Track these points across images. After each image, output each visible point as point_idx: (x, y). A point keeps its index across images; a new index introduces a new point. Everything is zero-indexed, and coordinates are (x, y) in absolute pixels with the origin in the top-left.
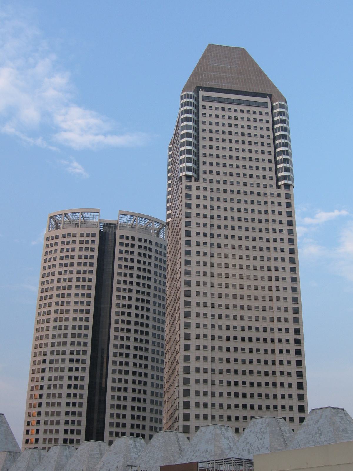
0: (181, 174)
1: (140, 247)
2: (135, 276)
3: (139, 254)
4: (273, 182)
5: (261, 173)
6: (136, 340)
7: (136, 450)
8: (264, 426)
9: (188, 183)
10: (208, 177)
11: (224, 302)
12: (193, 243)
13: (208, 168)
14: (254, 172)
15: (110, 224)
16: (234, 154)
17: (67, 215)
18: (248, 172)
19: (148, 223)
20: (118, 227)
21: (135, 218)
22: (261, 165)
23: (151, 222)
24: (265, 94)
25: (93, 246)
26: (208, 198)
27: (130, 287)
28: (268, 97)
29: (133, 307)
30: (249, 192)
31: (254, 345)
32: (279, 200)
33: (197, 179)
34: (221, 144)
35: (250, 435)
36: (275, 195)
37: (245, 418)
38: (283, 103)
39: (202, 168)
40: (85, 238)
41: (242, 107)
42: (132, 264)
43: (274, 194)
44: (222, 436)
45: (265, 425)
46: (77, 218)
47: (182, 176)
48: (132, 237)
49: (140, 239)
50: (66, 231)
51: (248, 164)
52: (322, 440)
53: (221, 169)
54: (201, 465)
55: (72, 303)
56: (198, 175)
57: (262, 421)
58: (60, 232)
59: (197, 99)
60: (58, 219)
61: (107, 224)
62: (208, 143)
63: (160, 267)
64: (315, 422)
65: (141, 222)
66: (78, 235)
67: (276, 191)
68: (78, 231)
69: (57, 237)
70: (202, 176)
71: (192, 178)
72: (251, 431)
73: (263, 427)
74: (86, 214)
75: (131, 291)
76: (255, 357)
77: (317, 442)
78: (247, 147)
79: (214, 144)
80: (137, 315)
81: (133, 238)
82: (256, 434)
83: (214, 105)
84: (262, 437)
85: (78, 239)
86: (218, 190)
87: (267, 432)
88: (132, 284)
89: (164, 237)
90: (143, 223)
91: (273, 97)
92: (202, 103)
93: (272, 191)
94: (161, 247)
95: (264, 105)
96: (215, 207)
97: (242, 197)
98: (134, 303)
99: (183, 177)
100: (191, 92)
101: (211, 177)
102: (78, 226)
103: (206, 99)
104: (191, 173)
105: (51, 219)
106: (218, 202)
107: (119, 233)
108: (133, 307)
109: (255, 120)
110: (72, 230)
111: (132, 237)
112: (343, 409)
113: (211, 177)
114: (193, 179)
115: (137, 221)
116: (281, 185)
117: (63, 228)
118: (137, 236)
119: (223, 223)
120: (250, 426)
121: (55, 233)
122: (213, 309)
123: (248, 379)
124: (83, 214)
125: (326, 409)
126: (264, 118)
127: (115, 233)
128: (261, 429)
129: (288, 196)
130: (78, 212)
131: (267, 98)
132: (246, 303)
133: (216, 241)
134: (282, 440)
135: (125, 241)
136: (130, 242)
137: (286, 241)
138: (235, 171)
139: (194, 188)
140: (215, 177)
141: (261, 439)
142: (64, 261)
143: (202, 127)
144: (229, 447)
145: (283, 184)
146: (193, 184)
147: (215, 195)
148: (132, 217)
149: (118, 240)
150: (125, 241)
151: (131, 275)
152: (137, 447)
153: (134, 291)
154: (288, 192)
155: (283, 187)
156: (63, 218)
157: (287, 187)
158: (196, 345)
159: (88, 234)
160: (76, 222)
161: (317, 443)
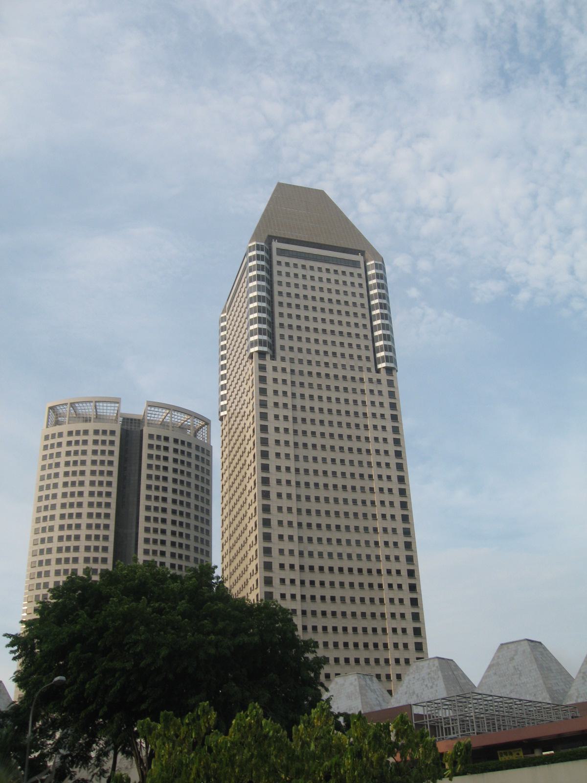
0: (252, 350)
1: (176, 451)
2: (170, 490)
3: (175, 461)
4: (371, 365)
5: (355, 352)
6: (175, 491)
8: (433, 669)
9: (262, 362)
10: (288, 355)
11: (314, 520)
12: (271, 442)
13: (287, 343)
14: (347, 351)
15: (132, 420)
16: (320, 326)
17: (73, 405)
20: (146, 424)
21: (168, 411)
22: (354, 341)
23: (189, 417)
24: (355, 250)
25: (112, 448)
26: (289, 382)
27: (163, 527)
29: (169, 511)
30: (340, 376)
31: (357, 579)
32: (380, 388)
33: (273, 357)
34: (302, 313)
35: (413, 683)
37: (407, 661)
38: (381, 263)
39: (279, 342)
40: (100, 438)
41: (327, 266)
42: (165, 474)
43: (373, 379)
44: (367, 688)
45: (435, 668)
46: (88, 410)
49: (176, 441)
50: (74, 427)
51: (338, 339)
52: (523, 681)
53: (305, 346)
54: (418, 710)
55: (84, 527)
56: (274, 351)
57: (429, 664)
58: (64, 428)
59: (269, 252)
60: (61, 410)
61: (128, 419)
62: (286, 311)
63: (203, 478)
64: (508, 660)
66: (91, 432)
67: (375, 376)
68: (91, 426)
69: (60, 435)
70: (279, 353)
72: (414, 678)
73: (431, 671)
74: (101, 404)
75: (164, 510)
76: (358, 594)
77: (517, 685)
78: (336, 318)
79: (294, 312)
80: (174, 522)
81: (166, 439)
82: (422, 681)
84: (433, 684)
85: (91, 438)
86: (301, 373)
87: (439, 677)
88: (167, 480)
90: (179, 418)
91: (366, 255)
92: (276, 258)
93: (370, 375)
95: (355, 264)
96: (298, 395)
97: (333, 383)
98: (169, 527)
99: (382, 369)
100: (263, 242)
101: (292, 355)
102: (90, 421)
103: (281, 252)
104: (265, 349)
105: (51, 410)
106: (302, 389)
107: (146, 431)
108: (169, 533)
109: (345, 283)
110: (82, 426)
112: (540, 643)
113: (292, 355)
114: (268, 357)
117: (69, 423)
118: (172, 436)
119: (309, 416)
120: (411, 671)
121: (57, 429)
122: (301, 530)
123: (350, 623)
124: (97, 404)
125: (522, 643)
126: (357, 281)
127: (142, 431)
128: (429, 674)
129: (391, 383)
130: (92, 402)
131: (358, 255)
133: (301, 440)
134: (458, 688)
135: (155, 442)
136: (163, 444)
137: (390, 441)
138: (322, 348)
139: (269, 368)
140: (296, 355)
141: (432, 687)
142: (71, 469)
143: (277, 289)
144: (378, 703)
146: (269, 363)
147: (298, 379)
148: (164, 411)
149: (146, 441)
151: (164, 500)
153: (169, 511)
154: (391, 378)
155: (383, 372)
156: (68, 409)
157: (389, 371)
159: (104, 432)
160: (85, 416)
161: (517, 687)
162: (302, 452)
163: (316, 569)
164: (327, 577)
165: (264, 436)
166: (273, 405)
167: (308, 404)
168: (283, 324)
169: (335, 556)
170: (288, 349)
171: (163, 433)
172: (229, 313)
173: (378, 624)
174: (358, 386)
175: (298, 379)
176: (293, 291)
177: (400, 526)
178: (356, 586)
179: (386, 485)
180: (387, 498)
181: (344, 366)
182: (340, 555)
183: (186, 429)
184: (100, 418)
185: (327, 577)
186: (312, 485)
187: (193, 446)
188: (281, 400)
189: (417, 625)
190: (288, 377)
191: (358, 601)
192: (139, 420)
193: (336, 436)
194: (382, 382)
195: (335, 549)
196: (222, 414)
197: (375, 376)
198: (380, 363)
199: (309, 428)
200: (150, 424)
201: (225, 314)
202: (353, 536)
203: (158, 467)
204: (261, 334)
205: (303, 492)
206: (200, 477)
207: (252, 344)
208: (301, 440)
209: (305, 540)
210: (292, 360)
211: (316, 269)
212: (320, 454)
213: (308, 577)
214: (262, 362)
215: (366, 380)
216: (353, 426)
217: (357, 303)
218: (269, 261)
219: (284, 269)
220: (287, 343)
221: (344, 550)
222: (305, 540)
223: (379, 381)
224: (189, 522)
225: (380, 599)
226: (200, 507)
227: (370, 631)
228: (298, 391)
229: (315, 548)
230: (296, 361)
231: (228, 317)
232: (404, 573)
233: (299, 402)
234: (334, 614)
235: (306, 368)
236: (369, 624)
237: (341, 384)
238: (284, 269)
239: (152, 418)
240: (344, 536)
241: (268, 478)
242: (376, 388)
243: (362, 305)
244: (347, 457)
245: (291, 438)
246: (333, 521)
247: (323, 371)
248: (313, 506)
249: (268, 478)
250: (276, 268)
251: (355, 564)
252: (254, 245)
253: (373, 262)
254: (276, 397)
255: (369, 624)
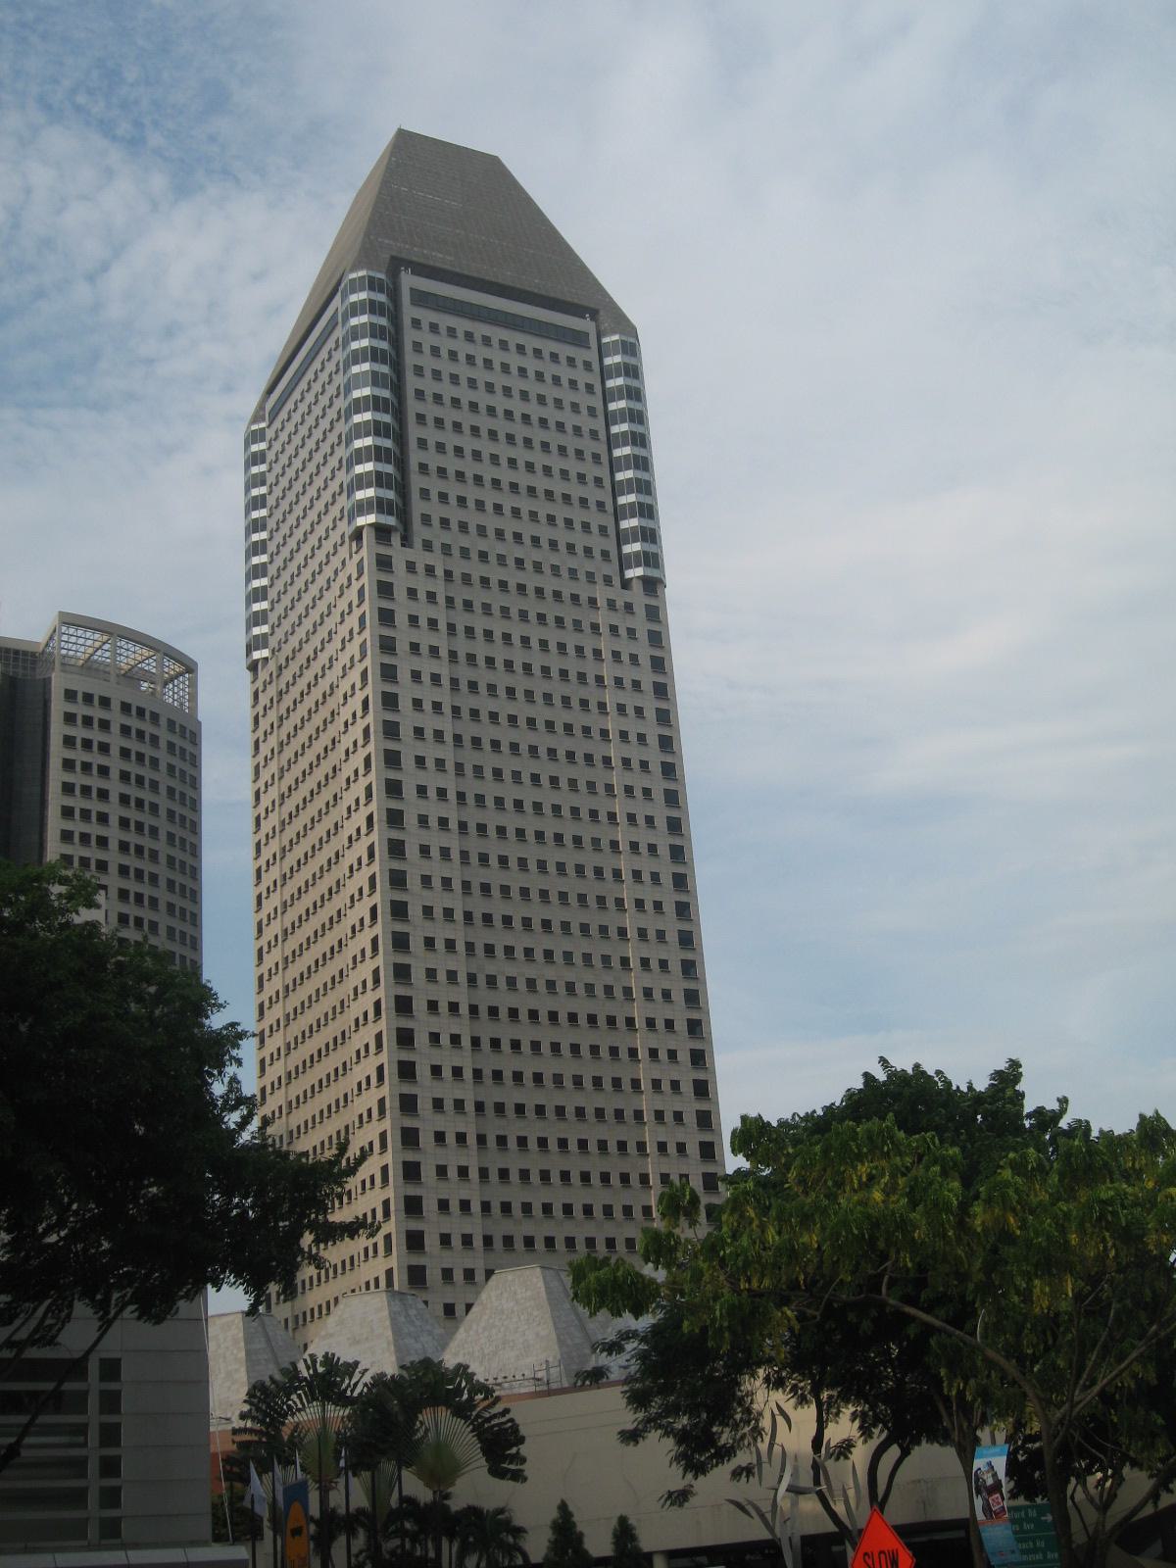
0: (361, 521)
4: (612, 569)
7: (412, 1329)
9: (383, 550)
10: (439, 537)
11: (498, 908)
15: (17, 652)
16: (506, 476)
18: (563, 537)
19: (97, 644)
28: (587, 315)
33: (406, 541)
36: (617, 607)
38: (632, 340)
39: (418, 507)
42: (103, 808)
47: (362, 527)
48: (101, 698)
49: (126, 708)
59: (394, 294)
63: (183, 795)
65: (73, 639)
67: (621, 597)
70: (420, 532)
71: (393, 534)
78: (538, 458)
81: (105, 702)
83: (446, 321)
89: (187, 697)
90: (130, 655)
92: (409, 311)
94: (183, 736)
95: (578, 339)
99: (634, 580)
100: (380, 272)
101: (446, 537)
103: (421, 299)
104: (391, 521)
107: (58, 683)
111: (101, 698)
113: (446, 537)
114: (396, 539)
115: (60, 637)
116: (632, 579)
123: (573, 1132)
131: (585, 318)
132: (556, 914)
133: (468, 730)
135: (80, 710)
136: (97, 713)
139: (399, 565)
145: (638, 577)
146: (399, 554)
149: (58, 707)
150: (80, 710)
151: (104, 748)
152: (413, 1322)
155: (637, 587)
158: (430, 1033)
162: (470, 758)
163: (503, 1013)
164: (526, 1033)
165: (390, 717)
166: (407, 648)
167: (481, 650)
168: (481, 477)
169: (541, 986)
170: (457, 529)
171: (98, 689)
172: (277, 424)
173: (628, 1133)
174: (587, 617)
175: (461, 594)
176: (448, 390)
177: (672, 926)
178: (545, 1048)
179: (644, 837)
180: (646, 865)
181: (555, 569)
182: (531, 984)
183: (139, 680)
184: (97, 670)
185: (526, 1033)
186: (492, 832)
187: (163, 721)
188: (426, 639)
189: (707, 1137)
190: (439, 587)
191: (607, 1084)
192: (33, 654)
193: (484, 716)
194: (636, 608)
195: (542, 972)
196: (256, 655)
197: (621, 597)
198: (630, 567)
199: (484, 704)
200: (66, 665)
201: (263, 425)
202: (579, 946)
203: (86, 767)
204: (382, 487)
205: (475, 845)
206: (177, 793)
207: (362, 508)
208: (468, 730)
209: (480, 950)
210: (446, 549)
211: (425, 326)
212: (508, 763)
213: (487, 1030)
214: (383, 550)
215: (601, 602)
216: (501, 692)
217: (497, 409)
218: (395, 318)
219: (428, 340)
220: (437, 511)
221: (560, 974)
222: (480, 950)
223: (629, 607)
224: (156, 895)
225: (633, 1080)
226: (177, 861)
227: (612, 1147)
228: (462, 620)
229: (501, 968)
230: (456, 552)
231: (270, 434)
232: (681, 1026)
233: (462, 646)
234: (520, 1109)
235: (477, 570)
236: (612, 1134)
237: (551, 610)
238: (428, 340)
239: (71, 653)
240: (559, 944)
241: (401, 812)
242: (623, 622)
243: (594, 434)
244: (565, 772)
245: (446, 724)
246: (537, 912)
247: (514, 578)
248: (495, 877)
249: (401, 812)
250: (410, 336)
251: (583, 1006)
252: (363, 277)
253: (616, 337)
254: (413, 630)
255: (612, 1134)
